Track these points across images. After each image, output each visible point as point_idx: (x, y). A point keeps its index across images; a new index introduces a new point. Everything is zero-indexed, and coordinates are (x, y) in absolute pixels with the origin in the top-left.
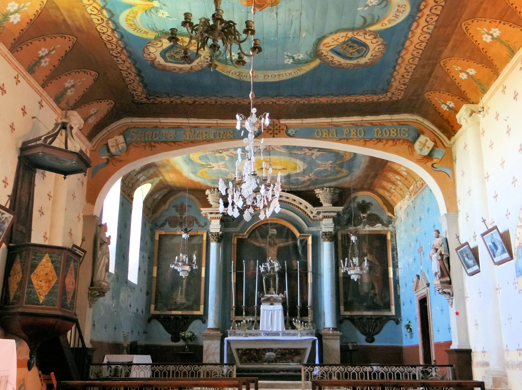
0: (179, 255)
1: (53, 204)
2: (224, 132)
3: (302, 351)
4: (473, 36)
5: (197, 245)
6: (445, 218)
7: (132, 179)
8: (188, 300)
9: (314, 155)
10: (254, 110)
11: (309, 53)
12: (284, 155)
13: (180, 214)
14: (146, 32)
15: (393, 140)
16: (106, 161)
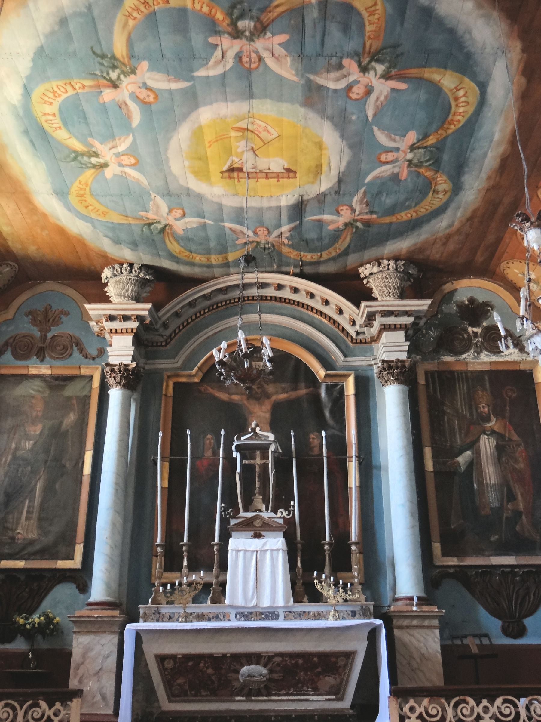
3: (341, 662)
8: (45, 533)
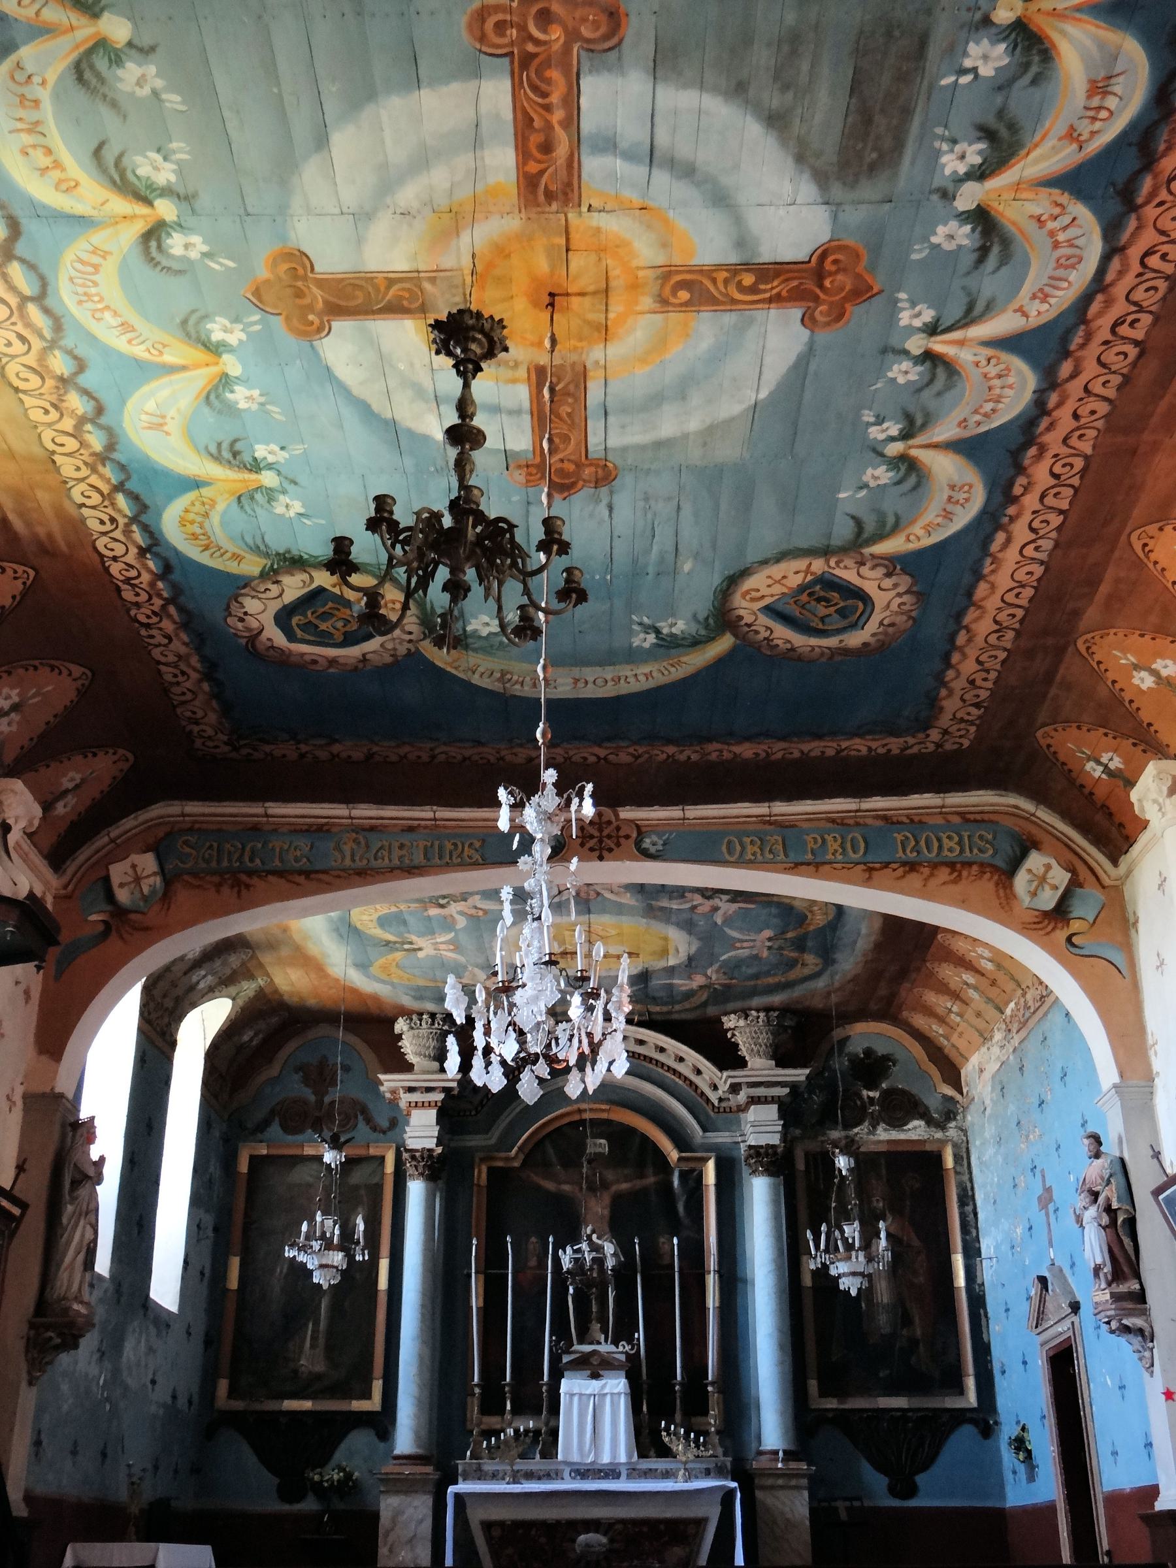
0: (312, 1220)
2: (455, 845)
3: (691, 1530)
4: (1163, 570)
5: (368, 1187)
6: (1116, 1099)
7: (174, 985)
9: (720, 912)
10: (549, 776)
11: (701, 616)
13: (315, 1093)
14: (236, 557)
15: (951, 865)
16: (101, 927)
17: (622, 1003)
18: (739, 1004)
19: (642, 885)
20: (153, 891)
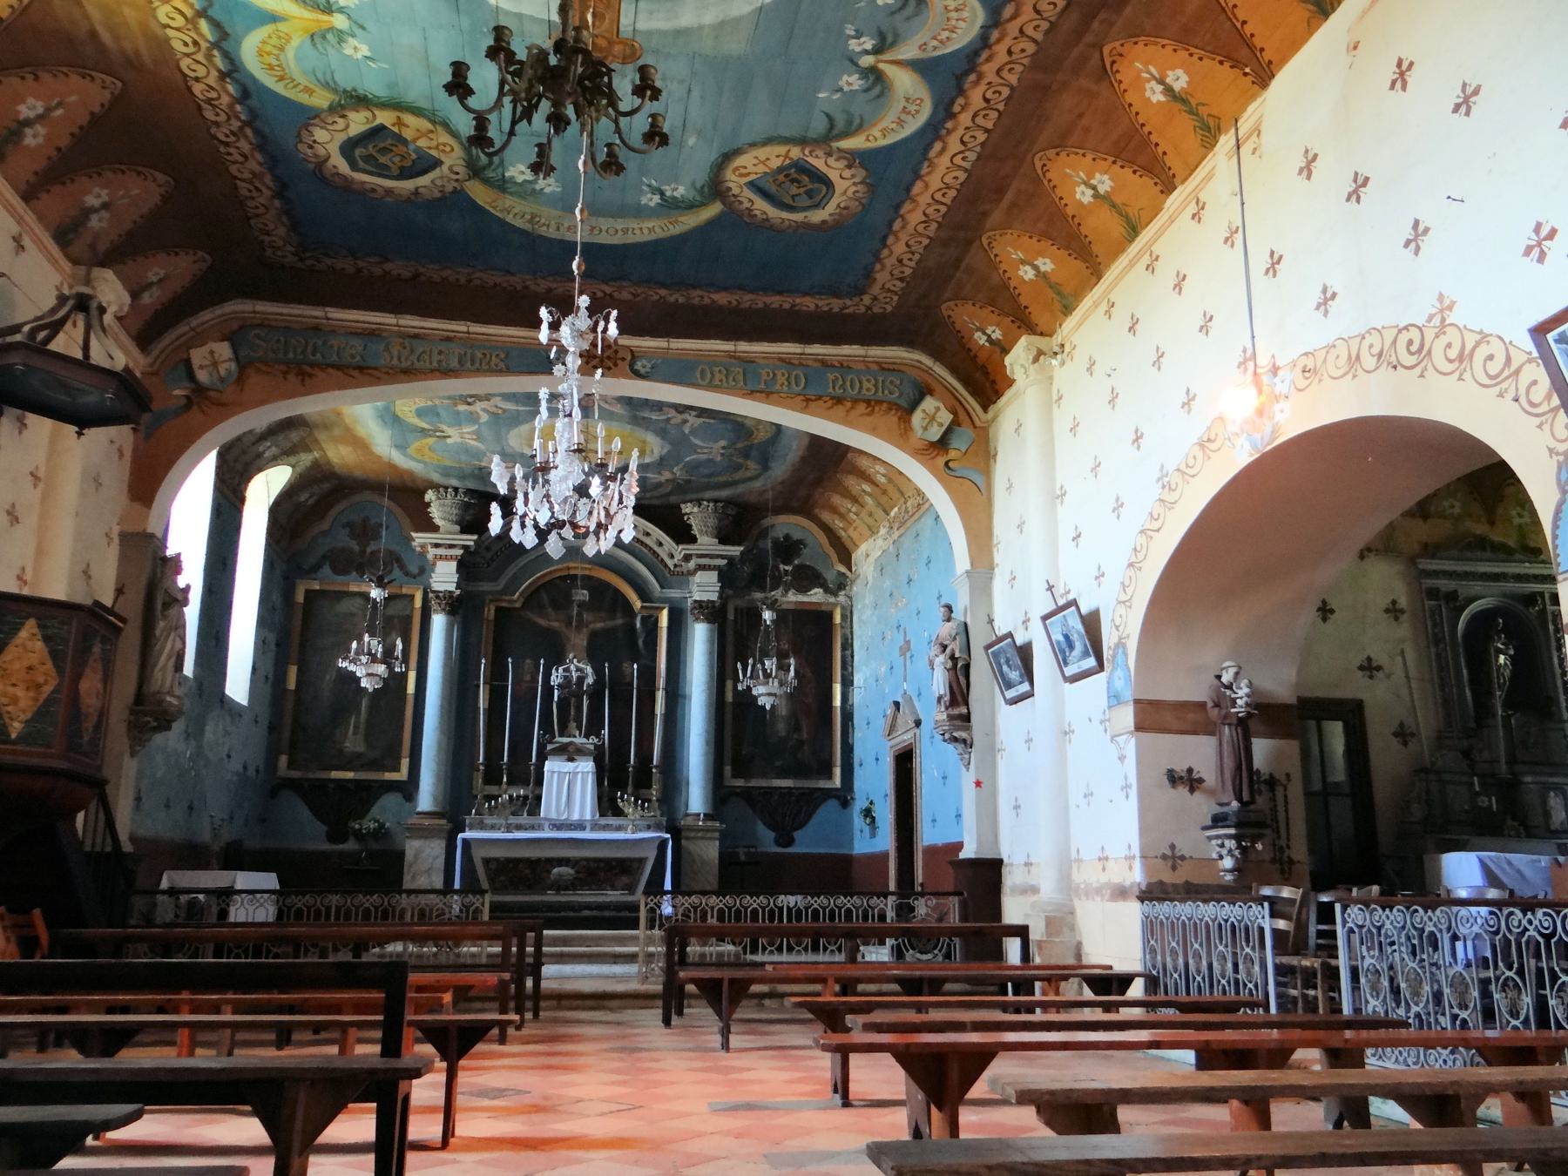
0: (360, 640)
1: (45, 498)
3: (635, 865)
10: (583, 301)
12: (619, 418)
14: (307, 90)
15: (868, 402)
16: (183, 401)
17: (630, 489)
18: (694, 496)
19: (631, 398)
20: (229, 371)
